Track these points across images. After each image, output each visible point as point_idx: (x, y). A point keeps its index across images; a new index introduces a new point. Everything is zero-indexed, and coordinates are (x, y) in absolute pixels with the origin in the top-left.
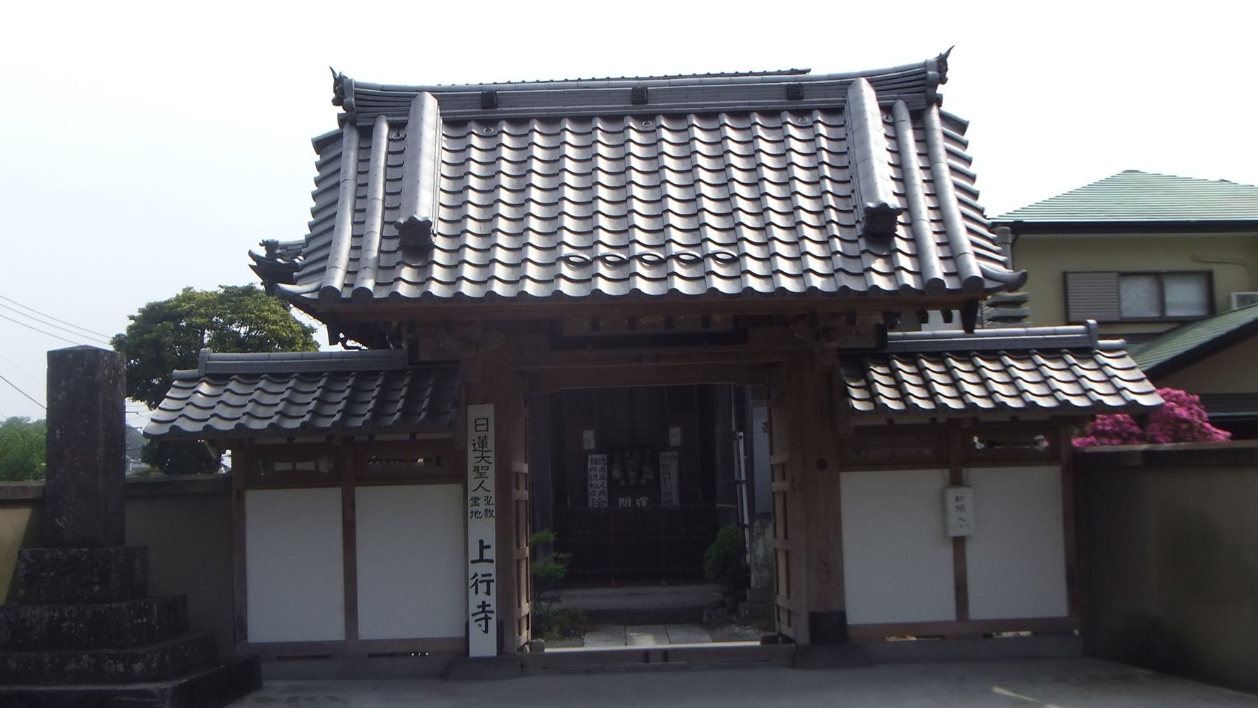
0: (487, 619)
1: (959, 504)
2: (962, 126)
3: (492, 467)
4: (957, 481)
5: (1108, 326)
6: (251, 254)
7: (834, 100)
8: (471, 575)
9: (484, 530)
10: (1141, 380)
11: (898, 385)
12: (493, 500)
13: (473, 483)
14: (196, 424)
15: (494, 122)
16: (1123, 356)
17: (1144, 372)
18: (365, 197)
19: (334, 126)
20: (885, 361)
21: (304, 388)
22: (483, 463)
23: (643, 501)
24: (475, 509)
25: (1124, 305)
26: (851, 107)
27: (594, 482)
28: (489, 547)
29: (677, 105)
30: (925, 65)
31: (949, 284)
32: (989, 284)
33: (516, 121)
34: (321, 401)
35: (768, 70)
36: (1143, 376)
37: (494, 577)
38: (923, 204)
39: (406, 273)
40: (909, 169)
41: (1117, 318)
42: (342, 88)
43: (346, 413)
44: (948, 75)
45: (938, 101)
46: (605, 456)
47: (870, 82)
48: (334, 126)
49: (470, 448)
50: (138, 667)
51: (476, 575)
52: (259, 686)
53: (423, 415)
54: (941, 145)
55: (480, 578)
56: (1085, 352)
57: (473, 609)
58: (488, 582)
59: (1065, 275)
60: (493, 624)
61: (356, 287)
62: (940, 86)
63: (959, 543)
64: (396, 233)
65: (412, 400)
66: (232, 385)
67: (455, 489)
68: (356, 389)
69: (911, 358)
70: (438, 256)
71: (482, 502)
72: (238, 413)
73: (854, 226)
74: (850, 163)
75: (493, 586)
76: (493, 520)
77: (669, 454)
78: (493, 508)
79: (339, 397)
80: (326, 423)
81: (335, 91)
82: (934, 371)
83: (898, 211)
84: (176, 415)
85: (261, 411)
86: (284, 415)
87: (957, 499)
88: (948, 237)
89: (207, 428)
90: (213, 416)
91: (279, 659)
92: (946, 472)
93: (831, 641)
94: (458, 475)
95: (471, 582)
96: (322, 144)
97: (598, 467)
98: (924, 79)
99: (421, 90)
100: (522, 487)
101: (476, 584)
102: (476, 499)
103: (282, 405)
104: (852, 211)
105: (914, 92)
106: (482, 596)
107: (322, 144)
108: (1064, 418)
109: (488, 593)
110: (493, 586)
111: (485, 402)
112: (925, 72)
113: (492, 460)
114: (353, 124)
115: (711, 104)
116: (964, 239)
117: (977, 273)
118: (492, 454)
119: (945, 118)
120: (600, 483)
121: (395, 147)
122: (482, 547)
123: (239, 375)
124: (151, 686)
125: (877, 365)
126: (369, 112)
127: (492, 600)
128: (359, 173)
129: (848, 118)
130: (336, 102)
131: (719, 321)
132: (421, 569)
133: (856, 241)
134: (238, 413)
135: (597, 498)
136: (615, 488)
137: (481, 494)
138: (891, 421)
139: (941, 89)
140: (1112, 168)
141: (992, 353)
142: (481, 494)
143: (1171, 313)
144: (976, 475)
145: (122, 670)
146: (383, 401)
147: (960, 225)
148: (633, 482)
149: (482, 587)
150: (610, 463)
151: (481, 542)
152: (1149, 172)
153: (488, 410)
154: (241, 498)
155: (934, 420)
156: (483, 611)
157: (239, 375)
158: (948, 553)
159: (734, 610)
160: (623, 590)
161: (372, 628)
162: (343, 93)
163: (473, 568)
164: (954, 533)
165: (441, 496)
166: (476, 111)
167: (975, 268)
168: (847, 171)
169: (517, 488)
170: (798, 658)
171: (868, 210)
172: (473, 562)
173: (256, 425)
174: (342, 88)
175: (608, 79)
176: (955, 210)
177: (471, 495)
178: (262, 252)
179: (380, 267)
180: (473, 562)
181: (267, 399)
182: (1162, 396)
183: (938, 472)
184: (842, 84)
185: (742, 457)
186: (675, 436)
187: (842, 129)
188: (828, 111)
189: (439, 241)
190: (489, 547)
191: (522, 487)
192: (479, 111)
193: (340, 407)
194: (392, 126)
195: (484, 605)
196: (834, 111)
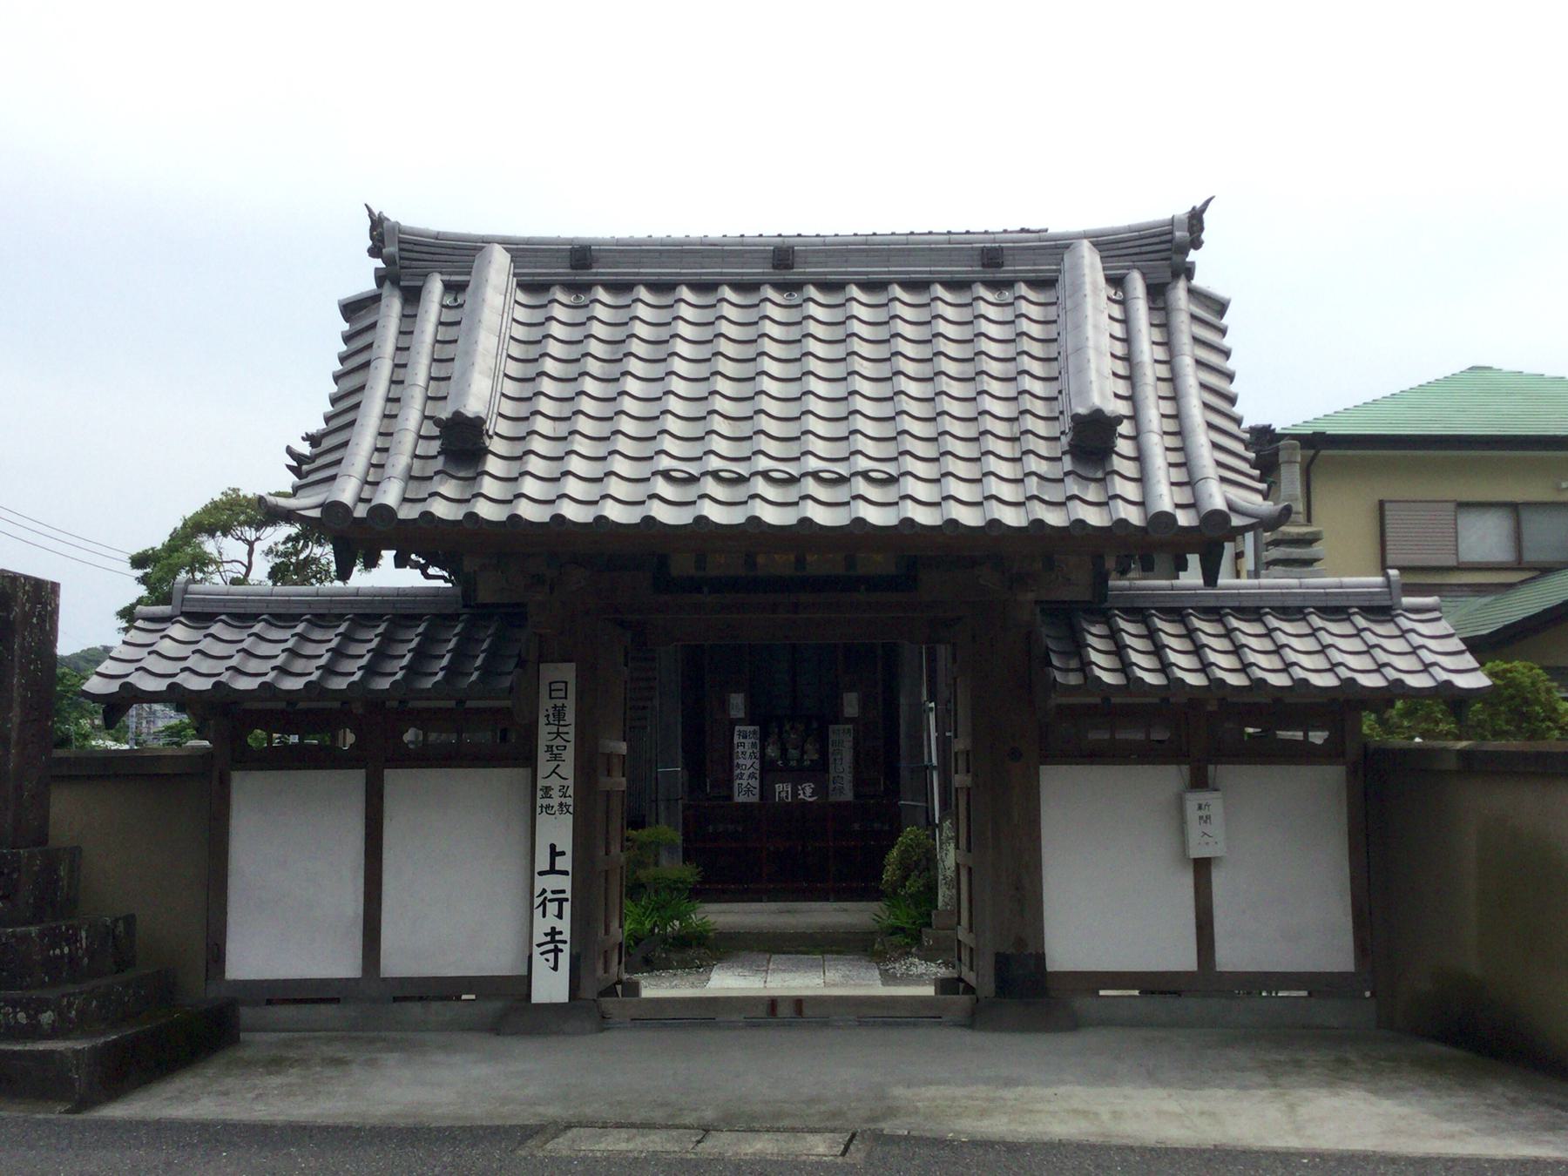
0: (557, 951)
1: (1203, 813)
2: (1220, 307)
3: (571, 747)
4: (1199, 782)
5: (1422, 577)
6: (289, 451)
7: (1046, 268)
8: (537, 891)
9: (557, 831)
10: (1462, 652)
11: (1119, 651)
12: (570, 792)
13: (544, 766)
14: (159, 680)
15: (586, 287)
16: (1438, 619)
17: (1464, 640)
18: (402, 382)
19: (368, 285)
20: (1105, 617)
21: (317, 634)
22: (559, 742)
23: (807, 792)
24: (545, 802)
25: (1462, 547)
26: (1066, 279)
27: (741, 761)
28: (563, 853)
29: (831, 271)
30: (1172, 222)
31: (1184, 519)
32: (1236, 521)
33: (617, 287)
34: (338, 653)
35: (1032, 228)
36: (1462, 647)
37: (568, 895)
38: (1154, 413)
39: (449, 488)
40: (1140, 364)
41: (1452, 562)
42: (381, 232)
43: (371, 670)
44: (1204, 236)
45: (1189, 271)
46: (757, 728)
47: (1095, 245)
48: (368, 285)
49: (542, 720)
50: (47, 1017)
51: (544, 891)
52: (234, 1041)
53: (473, 678)
54: (1184, 329)
55: (549, 895)
56: (1381, 611)
57: (539, 937)
58: (561, 901)
59: (1381, 504)
60: (564, 959)
61: (374, 503)
62: (1192, 252)
63: (1202, 868)
64: (436, 431)
65: (461, 655)
66: (216, 629)
67: (519, 774)
68: (388, 639)
69: (1138, 613)
70: (493, 465)
71: (555, 793)
72: (219, 667)
73: (1058, 439)
74: (1059, 358)
75: (567, 907)
76: (568, 820)
77: (841, 727)
78: (570, 801)
79: (362, 649)
80: (340, 684)
81: (372, 238)
82: (1168, 631)
83: (1119, 420)
84: (131, 667)
85: (253, 666)
86: (283, 671)
87: (1200, 807)
88: (1187, 456)
89: (172, 686)
90: (183, 670)
91: (269, 1002)
92: (1185, 768)
93: (1019, 992)
94: (526, 758)
95: (537, 901)
96: (350, 309)
97: (748, 742)
98: (1170, 241)
99: (488, 241)
100: (617, 771)
101: (543, 903)
102: (547, 789)
103: (283, 657)
104: (1057, 419)
105: (1158, 258)
106: (551, 921)
107: (350, 309)
108: (1346, 703)
109: (560, 916)
110: (567, 907)
111: (566, 659)
112: (1171, 233)
113: (571, 737)
114: (395, 282)
115: (877, 271)
116: (1205, 457)
117: (1219, 504)
118: (572, 729)
119: (1193, 293)
120: (749, 763)
121: (449, 316)
122: (554, 853)
123: (228, 614)
124: (59, 1045)
125: (1093, 623)
126: (411, 263)
127: (564, 926)
128: (398, 349)
129: (1061, 293)
130: (374, 252)
131: (878, 563)
132: (473, 883)
133: (1060, 459)
134: (219, 667)
135: (745, 783)
136: (768, 771)
137: (555, 782)
138: (1106, 699)
139: (1193, 256)
140: (1453, 363)
141: (1252, 611)
142: (555, 782)
143: (1530, 556)
144: (1224, 773)
145: (24, 1021)
146: (422, 655)
147: (1201, 440)
148: (793, 763)
149: (552, 908)
150: (764, 738)
151: (553, 847)
152: (1506, 368)
153: (568, 672)
154: (225, 782)
155: (1165, 700)
156: (553, 941)
157: (228, 614)
158: (1186, 883)
159: (917, 939)
160: (773, 906)
161: (397, 962)
162: (382, 241)
163: (541, 883)
164: (1196, 852)
165: (501, 781)
166: (564, 271)
167: (1216, 496)
168: (1055, 364)
169: (609, 774)
170: (979, 1016)
171: (1076, 418)
172: (541, 873)
173: (244, 684)
174: (381, 232)
175: (949, 233)
176: (1196, 414)
177: (541, 783)
178: (305, 449)
179: (412, 478)
180: (541, 873)
181: (264, 649)
182: (1491, 674)
183: (1173, 769)
184: (1056, 247)
185: (933, 735)
186: (851, 704)
187: (1054, 308)
188: (1034, 284)
189: (496, 445)
190: (563, 853)
191: (617, 771)
192: (565, 271)
193: (363, 662)
194: (449, 287)
195: (553, 932)
196: (1044, 283)
